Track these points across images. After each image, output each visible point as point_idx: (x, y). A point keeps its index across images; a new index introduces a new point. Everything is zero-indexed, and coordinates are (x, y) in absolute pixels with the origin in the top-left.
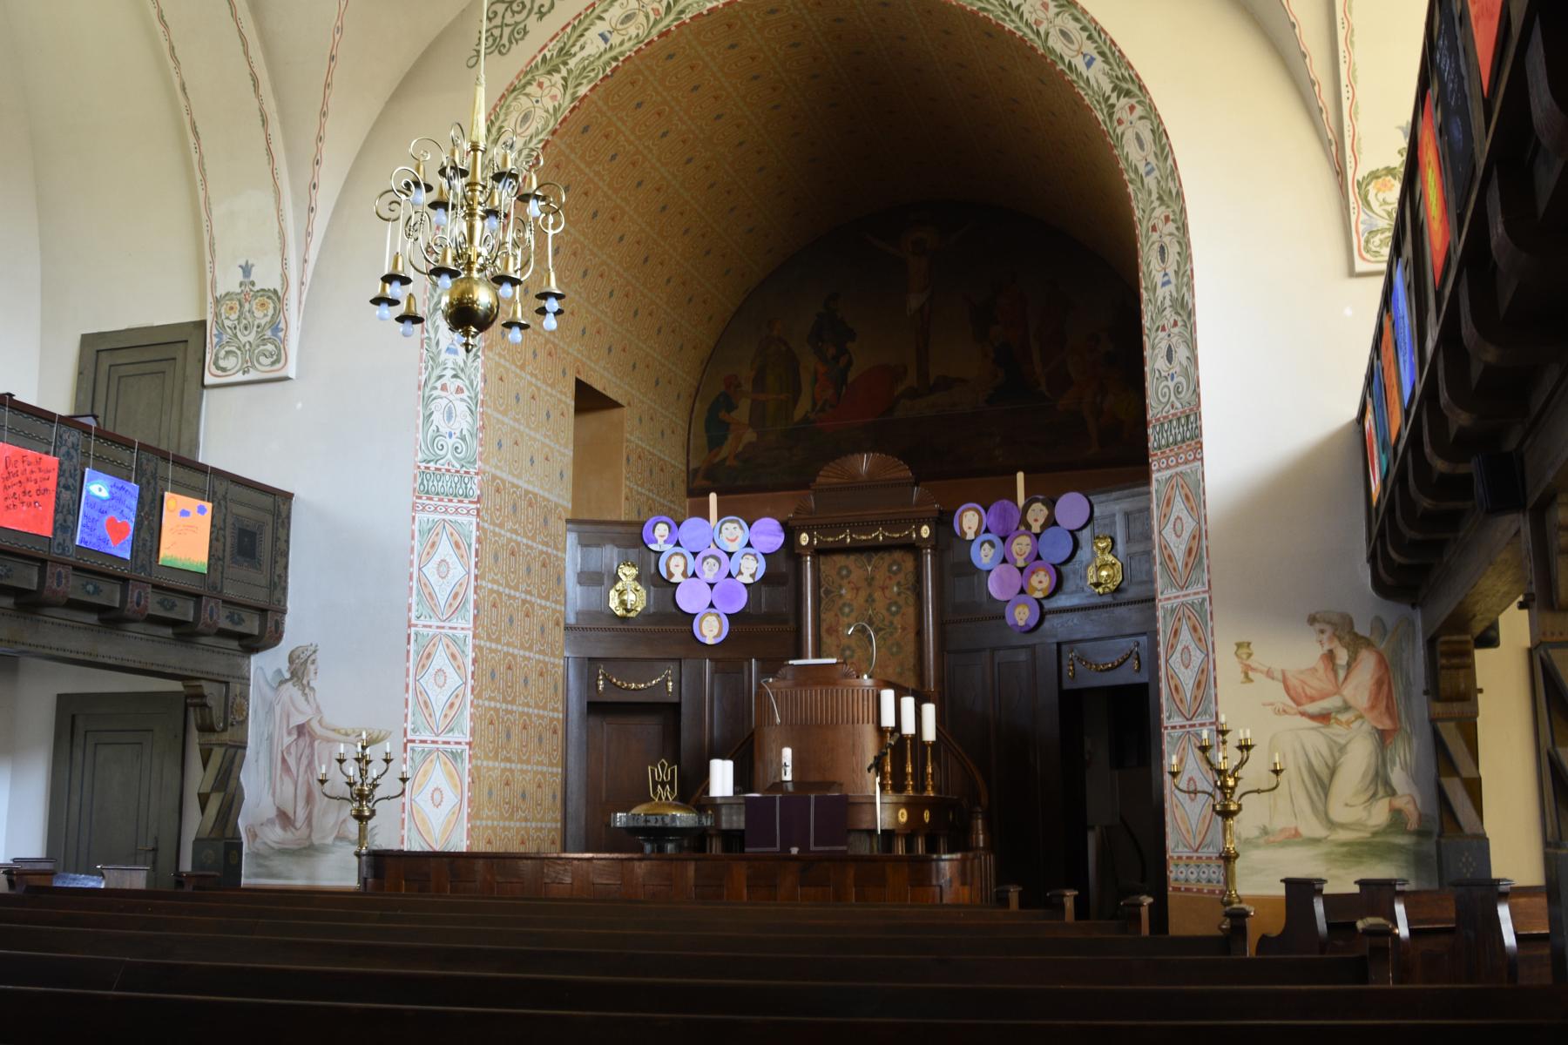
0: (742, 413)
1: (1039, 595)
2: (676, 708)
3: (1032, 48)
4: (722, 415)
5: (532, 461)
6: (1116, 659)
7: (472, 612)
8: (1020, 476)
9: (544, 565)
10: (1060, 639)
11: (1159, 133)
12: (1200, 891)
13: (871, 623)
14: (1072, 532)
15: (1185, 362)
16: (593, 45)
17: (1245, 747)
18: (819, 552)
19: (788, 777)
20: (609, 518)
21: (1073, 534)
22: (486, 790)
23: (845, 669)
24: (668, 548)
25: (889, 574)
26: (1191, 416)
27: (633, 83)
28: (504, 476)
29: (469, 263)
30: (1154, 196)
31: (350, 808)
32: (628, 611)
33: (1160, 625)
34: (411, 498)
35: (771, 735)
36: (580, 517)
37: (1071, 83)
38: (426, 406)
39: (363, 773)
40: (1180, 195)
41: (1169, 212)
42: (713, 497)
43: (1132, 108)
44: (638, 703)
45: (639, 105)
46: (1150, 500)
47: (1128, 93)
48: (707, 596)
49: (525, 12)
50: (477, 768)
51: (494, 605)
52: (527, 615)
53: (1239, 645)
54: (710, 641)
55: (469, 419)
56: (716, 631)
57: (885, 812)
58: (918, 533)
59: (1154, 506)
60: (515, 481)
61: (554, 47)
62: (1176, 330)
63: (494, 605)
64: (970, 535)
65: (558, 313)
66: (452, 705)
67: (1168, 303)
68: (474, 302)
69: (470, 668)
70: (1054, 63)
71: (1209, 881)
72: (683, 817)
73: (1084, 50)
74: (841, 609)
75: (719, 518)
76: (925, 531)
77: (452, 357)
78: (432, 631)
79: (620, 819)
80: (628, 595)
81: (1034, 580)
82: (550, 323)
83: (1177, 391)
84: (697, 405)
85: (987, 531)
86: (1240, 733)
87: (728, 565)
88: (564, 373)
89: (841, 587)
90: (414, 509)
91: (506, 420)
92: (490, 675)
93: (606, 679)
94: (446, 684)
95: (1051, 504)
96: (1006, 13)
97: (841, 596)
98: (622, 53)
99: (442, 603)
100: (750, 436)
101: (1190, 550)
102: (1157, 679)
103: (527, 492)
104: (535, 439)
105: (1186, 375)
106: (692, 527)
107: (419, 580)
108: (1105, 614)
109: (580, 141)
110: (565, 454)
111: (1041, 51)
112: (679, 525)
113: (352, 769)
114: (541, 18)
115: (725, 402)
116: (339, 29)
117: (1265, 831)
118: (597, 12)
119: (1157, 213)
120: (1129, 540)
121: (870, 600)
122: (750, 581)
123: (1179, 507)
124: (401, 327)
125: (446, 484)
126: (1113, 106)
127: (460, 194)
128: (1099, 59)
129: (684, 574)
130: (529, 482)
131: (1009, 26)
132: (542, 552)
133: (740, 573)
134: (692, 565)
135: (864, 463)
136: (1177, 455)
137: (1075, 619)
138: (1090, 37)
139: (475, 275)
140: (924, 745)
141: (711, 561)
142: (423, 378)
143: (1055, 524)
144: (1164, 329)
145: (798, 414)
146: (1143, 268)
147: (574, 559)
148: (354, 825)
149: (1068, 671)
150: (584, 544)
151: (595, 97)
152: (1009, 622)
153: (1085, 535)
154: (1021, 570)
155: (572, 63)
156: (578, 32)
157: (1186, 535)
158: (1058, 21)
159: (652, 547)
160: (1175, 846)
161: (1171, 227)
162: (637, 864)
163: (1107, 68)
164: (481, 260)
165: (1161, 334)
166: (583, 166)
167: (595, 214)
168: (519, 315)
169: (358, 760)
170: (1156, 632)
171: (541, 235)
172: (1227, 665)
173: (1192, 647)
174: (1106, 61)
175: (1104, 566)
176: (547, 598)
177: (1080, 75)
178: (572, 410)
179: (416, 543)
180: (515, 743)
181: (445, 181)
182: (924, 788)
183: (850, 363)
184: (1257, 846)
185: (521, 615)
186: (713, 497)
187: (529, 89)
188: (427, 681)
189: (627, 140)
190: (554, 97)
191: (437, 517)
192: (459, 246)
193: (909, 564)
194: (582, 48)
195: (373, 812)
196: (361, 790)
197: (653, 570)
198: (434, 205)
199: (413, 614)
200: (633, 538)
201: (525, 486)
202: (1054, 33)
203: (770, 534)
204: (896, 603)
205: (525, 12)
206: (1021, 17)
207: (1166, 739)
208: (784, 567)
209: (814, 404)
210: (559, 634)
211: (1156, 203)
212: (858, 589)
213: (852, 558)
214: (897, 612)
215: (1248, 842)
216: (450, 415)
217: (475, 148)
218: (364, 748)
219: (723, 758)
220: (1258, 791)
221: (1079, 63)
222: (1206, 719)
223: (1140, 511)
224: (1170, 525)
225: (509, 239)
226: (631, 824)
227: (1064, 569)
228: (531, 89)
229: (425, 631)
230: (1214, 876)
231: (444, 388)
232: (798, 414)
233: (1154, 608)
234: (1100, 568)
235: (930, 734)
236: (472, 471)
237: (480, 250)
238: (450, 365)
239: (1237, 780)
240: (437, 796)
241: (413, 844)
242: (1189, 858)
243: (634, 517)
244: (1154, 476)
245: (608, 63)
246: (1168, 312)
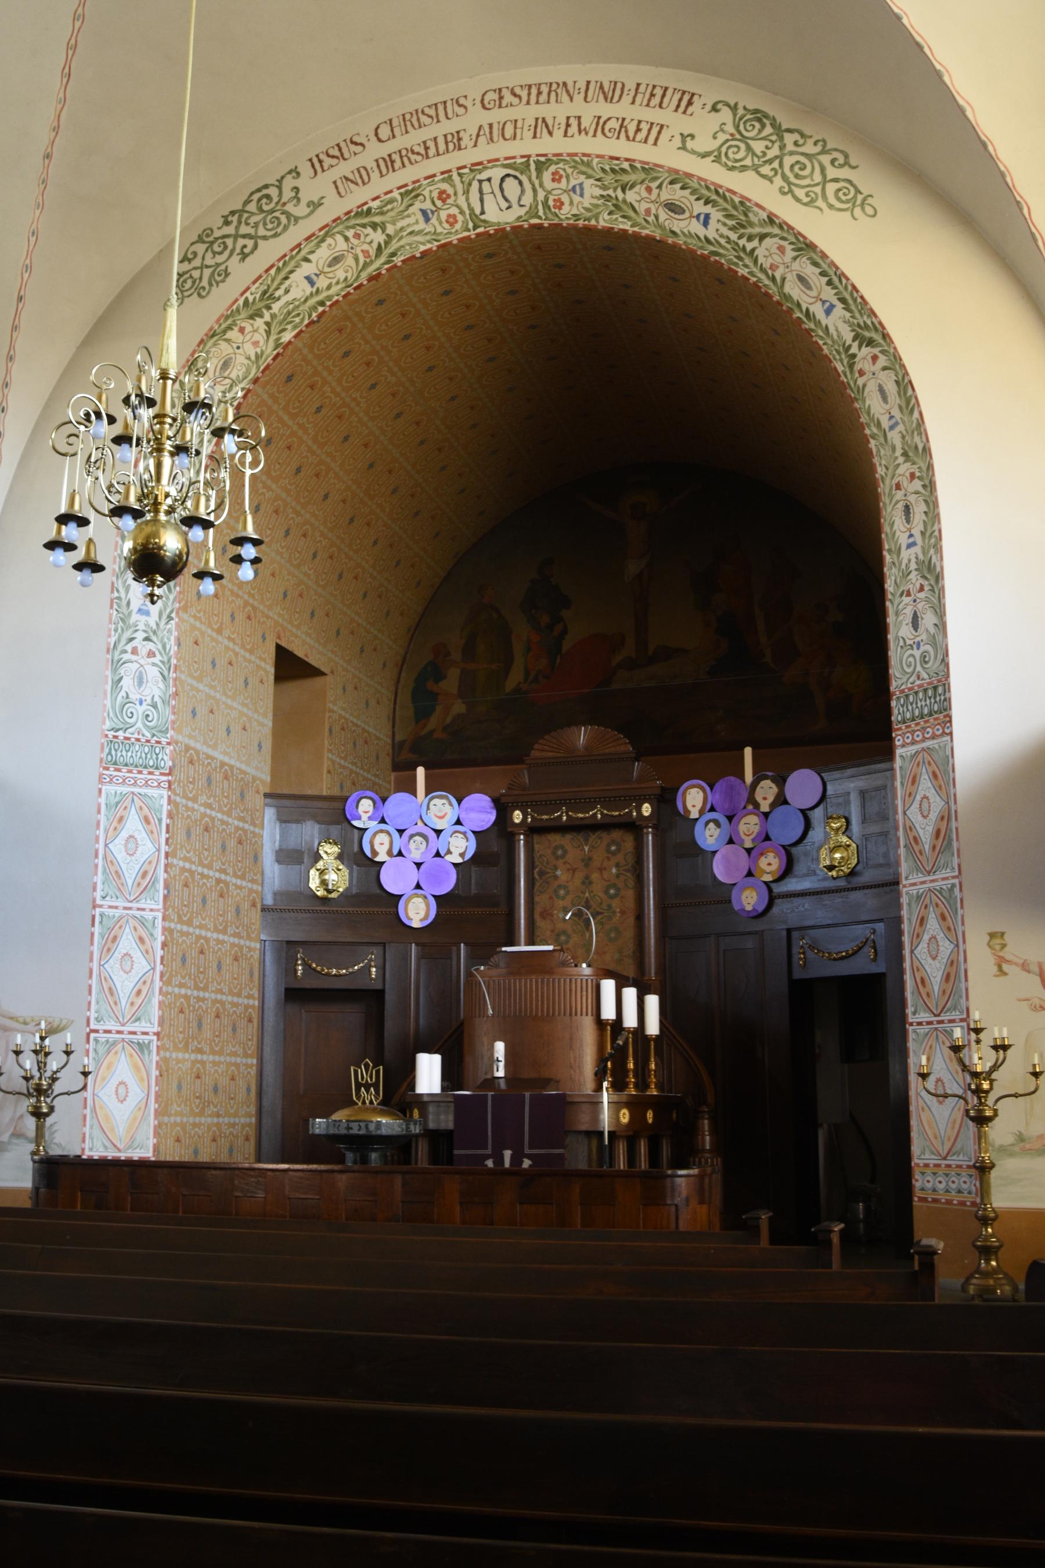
0: (451, 683)
1: (768, 878)
2: (379, 995)
3: (766, 294)
4: (430, 685)
5: (228, 731)
6: (851, 946)
7: (162, 891)
8: (748, 752)
9: (240, 842)
10: (791, 924)
11: (905, 384)
12: (949, 1202)
13: (588, 907)
14: (803, 811)
15: (932, 630)
16: (298, 288)
17: (1001, 1047)
18: (533, 830)
19: (501, 1073)
20: (309, 792)
22: (175, 1086)
23: (563, 956)
24: (373, 825)
25: (607, 855)
26: (938, 689)
27: (340, 331)
28: (198, 746)
29: (156, 504)
30: (899, 452)
31: (26, 1104)
32: (329, 891)
33: (904, 913)
34: (96, 769)
35: (482, 1028)
36: (279, 791)
37: (808, 331)
38: (115, 671)
39: (41, 1066)
40: (927, 451)
41: (914, 469)
42: (421, 771)
43: (875, 358)
44: (339, 991)
45: (346, 354)
46: (893, 778)
47: (870, 343)
48: (413, 876)
49: (227, 253)
50: (165, 1060)
51: (186, 885)
52: (221, 896)
53: (992, 935)
54: (416, 924)
55: (161, 685)
56: (422, 914)
57: (609, 1112)
58: (639, 812)
59: (898, 784)
60: (210, 752)
61: (257, 290)
62: (922, 595)
63: (186, 885)
64: (694, 814)
65: (255, 561)
66: (139, 992)
67: (913, 566)
68: (160, 548)
69: (159, 953)
70: (790, 311)
71: (959, 1192)
72: (387, 1124)
73: (823, 297)
74: (556, 891)
75: (427, 794)
76: (646, 809)
77: (144, 618)
78: (118, 913)
79: (319, 1125)
80: (330, 875)
81: (763, 863)
82: (246, 572)
83: (924, 661)
84: (403, 674)
85: (712, 809)
86: (996, 1032)
87: (437, 844)
88: (264, 638)
89: (556, 868)
90: (101, 782)
91: (201, 687)
92: (179, 959)
93: (305, 964)
94: (133, 969)
95: (781, 781)
96: (739, 258)
97: (556, 877)
98: (329, 298)
99: (130, 882)
100: (459, 707)
102: (901, 972)
103: (223, 764)
104: (231, 708)
105: (934, 643)
106: (398, 803)
107: (105, 857)
108: (838, 899)
109: (282, 382)
110: (263, 724)
111: (776, 298)
112: (384, 800)
113: (29, 1062)
114: (243, 259)
115: (434, 671)
116: (28, 268)
117: (1021, 1138)
118: (303, 253)
119: (901, 470)
120: (864, 820)
121: (587, 882)
122: (459, 860)
123: (925, 785)
124: (79, 576)
125: (135, 754)
126: (854, 356)
127: (147, 425)
128: (839, 306)
129: (390, 853)
130: (225, 753)
131: (742, 271)
132: (237, 828)
133: (449, 852)
134: (398, 843)
135: (582, 736)
136: (924, 729)
137: (806, 903)
138: (830, 283)
139: (162, 517)
140: (647, 1039)
141: (418, 838)
142: (113, 640)
143: (785, 802)
144: (909, 594)
145: (510, 684)
146: (886, 528)
147: (273, 835)
148: (31, 1122)
149: (798, 959)
150: (283, 819)
151: (300, 345)
152: (736, 907)
153: (817, 815)
154: (749, 851)
155: (276, 307)
156: (282, 275)
157: (933, 816)
158: (795, 266)
159: (356, 823)
160: (920, 1152)
161: (917, 485)
162: (338, 1176)
163: (848, 315)
164: (169, 501)
165: (906, 600)
166: (286, 418)
167: (298, 470)
168: (212, 564)
169: (36, 1052)
170: (899, 920)
171: (237, 475)
172: (979, 958)
173: (940, 936)
174: (847, 309)
175: (837, 847)
176: (243, 877)
177: (818, 323)
178: (272, 678)
179: (102, 818)
180: (207, 1034)
181: (129, 413)
182: (647, 1086)
183: (565, 631)
184: (1012, 1155)
185: (215, 895)
186: (421, 771)
187: (229, 335)
188: (113, 967)
189: (333, 391)
190: (256, 344)
191: (125, 789)
192: (143, 484)
193: (629, 844)
194: (287, 291)
195: (52, 1109)
196: (39, 1085)
197: (356, 848)
198: (119, 440)
199: (98, 894)
200: (335, 815)
201: (221, 757)
202: (791, 278)
203: (482, 811)
204: (614, 886)
205: (227, 253)
206: (756, 261)
207: (911, 1036)
208: (495, 846)
209: (527, 673)
210: (256, 915)
211: (901, 460)
212: (574, 870)
213: (568, 837)
214: (615, 896)
215: (1002, 1149)
216: (140, 681)
217: (164, 376)
218: (42, 1039)
219: (430, 1051)
220: (1016, 1096)
221: (818, 310)
222: (956, 1015)
223: (877, 789)
224: (916, 805)
225: (201, 478)
226: (332, 1131)
227: (794, 851)
228: (233, 334)
229: (111, 912)
230: (965, 1186)
231: (134, 651)
232: (510, 684)
233: (899, 895)
234: (834, 850)
235: (653, 1027)
236: (164, 740)
237: (168, 488)
238: (141, 627)
239: (992, 1081)
240: (122, 1091)
241: (95, 1149)
242: (936, 1166)
243: (336, 792)
244: (899, 752)
245: (314, 308)
246: (913, 576)
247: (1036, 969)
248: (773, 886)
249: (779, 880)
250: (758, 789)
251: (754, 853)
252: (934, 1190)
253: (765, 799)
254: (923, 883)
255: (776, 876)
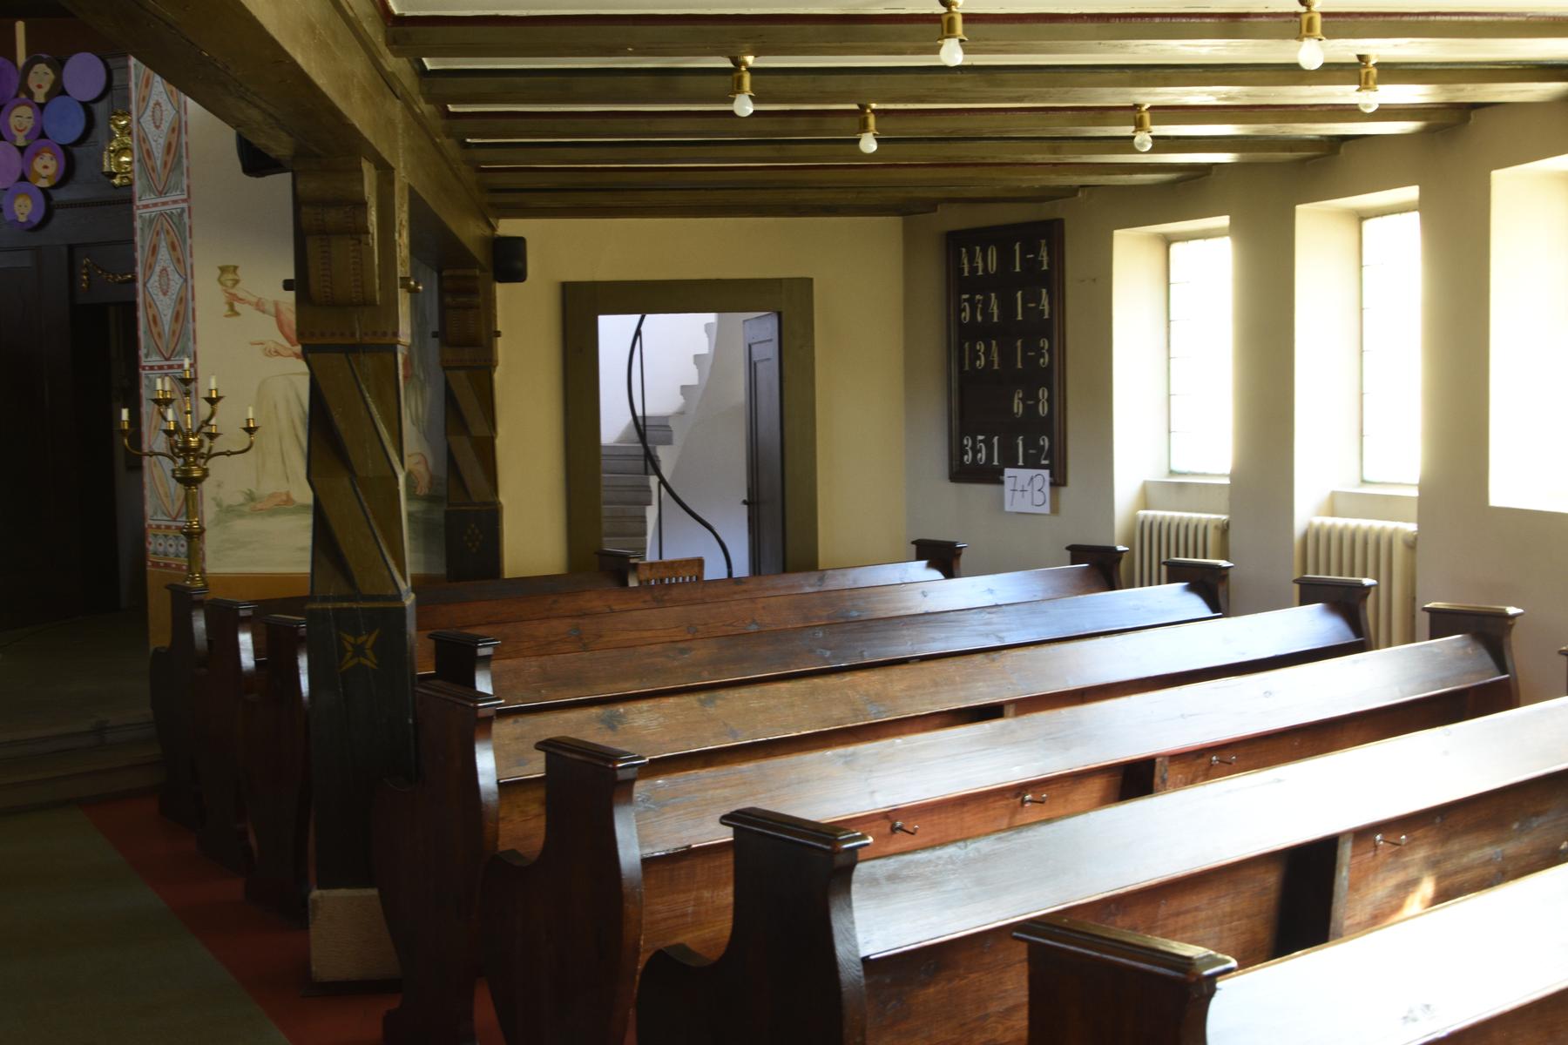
1: (44, 184)
8: (20, 27)
21: (86, 106)
33: (138, 239)
53: (223, 270)
59: (132, 85)
95: (58, 65)
101: (170, 145)
117: (251, 497)
143: (64, 92)
153: (100, 109)
157: (165, 126)
172: (208, 295)
173: (171, 269)
184: (241, 515)
195: (206, 473)
227: (76, 151)
247: (273, 310)
248: (52, 192)
249: (58, 185)
250: (32, 74)
251: (27, 153)
252: (166, 554)
253: (40, 87)
254: (155, 205)
255: (53, 182)
